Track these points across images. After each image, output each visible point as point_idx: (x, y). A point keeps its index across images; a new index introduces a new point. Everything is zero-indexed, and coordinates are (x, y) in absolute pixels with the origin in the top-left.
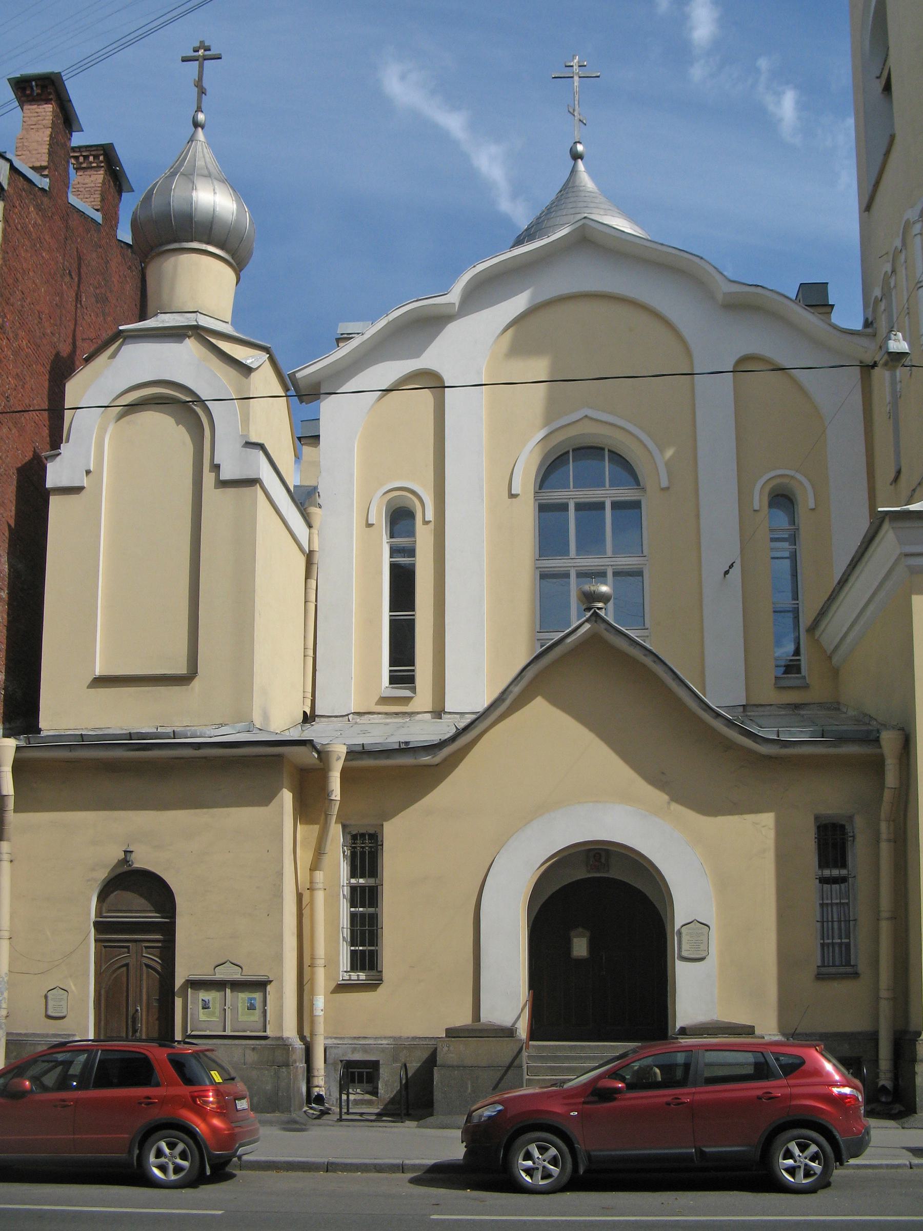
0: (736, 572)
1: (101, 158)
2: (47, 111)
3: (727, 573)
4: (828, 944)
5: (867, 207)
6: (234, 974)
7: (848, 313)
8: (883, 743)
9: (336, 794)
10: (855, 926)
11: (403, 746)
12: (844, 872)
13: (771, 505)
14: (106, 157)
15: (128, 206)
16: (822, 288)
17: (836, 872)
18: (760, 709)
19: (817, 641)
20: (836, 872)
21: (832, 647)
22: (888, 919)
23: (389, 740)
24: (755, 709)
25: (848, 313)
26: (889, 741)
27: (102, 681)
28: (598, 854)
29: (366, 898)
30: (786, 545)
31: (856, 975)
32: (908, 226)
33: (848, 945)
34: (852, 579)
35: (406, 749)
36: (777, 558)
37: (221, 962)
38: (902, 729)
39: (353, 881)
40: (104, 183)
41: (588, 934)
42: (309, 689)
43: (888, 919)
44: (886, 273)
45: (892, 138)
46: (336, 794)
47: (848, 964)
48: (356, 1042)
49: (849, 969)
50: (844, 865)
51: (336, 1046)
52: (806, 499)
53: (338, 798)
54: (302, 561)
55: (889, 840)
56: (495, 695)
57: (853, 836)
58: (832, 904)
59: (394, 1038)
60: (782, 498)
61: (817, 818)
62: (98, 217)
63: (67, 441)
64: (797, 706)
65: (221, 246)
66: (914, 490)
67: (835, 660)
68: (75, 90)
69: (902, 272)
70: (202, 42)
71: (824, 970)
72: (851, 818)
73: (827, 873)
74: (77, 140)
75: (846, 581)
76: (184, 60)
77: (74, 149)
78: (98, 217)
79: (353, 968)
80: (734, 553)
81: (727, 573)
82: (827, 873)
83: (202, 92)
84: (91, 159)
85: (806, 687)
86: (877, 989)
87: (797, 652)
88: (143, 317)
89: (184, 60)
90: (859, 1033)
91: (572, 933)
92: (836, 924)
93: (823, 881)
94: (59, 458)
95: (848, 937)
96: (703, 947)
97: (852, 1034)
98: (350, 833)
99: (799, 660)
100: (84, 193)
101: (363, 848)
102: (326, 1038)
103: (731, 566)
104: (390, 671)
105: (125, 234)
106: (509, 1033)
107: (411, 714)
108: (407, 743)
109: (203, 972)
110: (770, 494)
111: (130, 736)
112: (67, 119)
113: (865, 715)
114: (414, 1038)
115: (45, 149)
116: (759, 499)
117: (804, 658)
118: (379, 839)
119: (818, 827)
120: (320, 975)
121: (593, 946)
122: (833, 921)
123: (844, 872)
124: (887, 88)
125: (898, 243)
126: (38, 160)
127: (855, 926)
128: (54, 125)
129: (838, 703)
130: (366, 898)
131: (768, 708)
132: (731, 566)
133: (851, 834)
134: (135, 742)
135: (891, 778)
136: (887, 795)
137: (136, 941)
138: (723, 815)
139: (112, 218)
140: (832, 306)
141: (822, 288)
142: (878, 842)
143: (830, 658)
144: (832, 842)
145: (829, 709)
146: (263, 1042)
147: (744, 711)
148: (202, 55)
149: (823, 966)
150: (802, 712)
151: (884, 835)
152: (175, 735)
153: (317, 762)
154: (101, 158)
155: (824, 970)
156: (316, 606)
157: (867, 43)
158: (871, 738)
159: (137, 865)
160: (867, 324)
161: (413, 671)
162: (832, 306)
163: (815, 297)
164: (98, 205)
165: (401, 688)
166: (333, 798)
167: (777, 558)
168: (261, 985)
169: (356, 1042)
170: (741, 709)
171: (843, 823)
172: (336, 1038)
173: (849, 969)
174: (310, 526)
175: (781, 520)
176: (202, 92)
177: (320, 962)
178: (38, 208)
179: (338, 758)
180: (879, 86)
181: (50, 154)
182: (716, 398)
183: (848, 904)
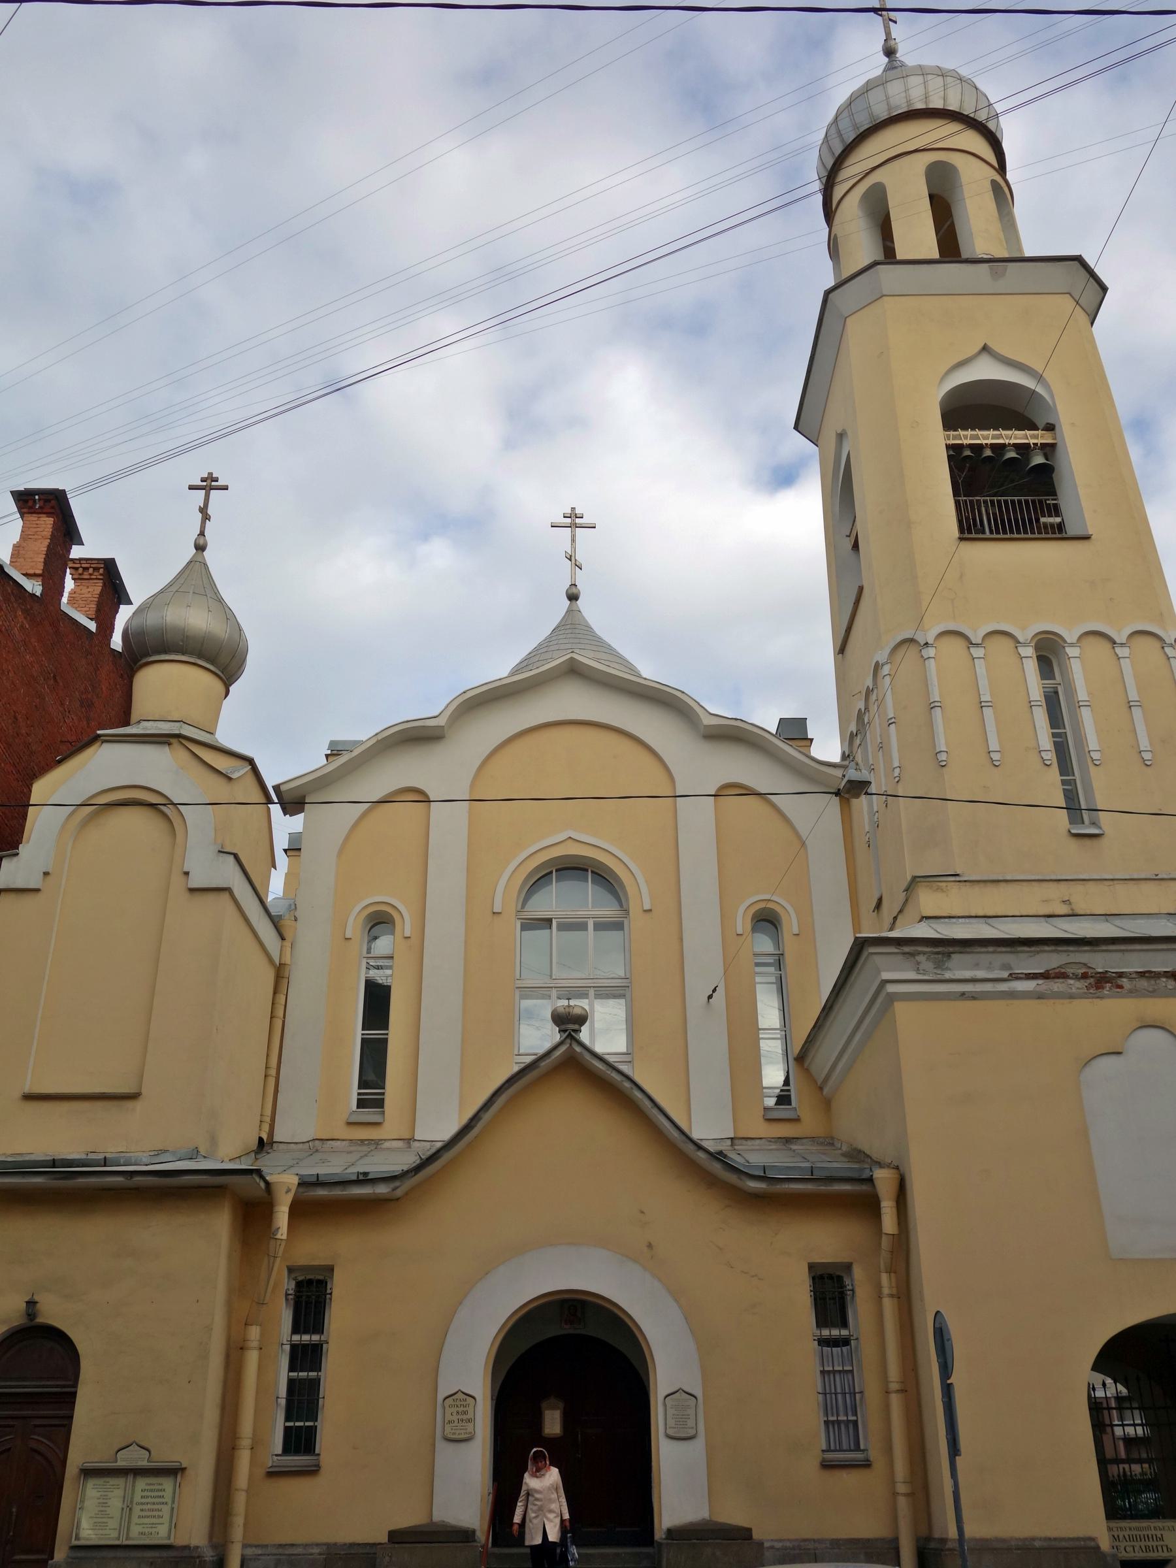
0: (720, 996)
1: (101, 571)
2: (47, 523)
3: (710, 997)
4: (833, 1422)
5: (842, 649)
6: (136, 1458)
7: (827, 747)
8: (878, 1184)
9: (283, 1232)
10: (862, 1399)
11: (361, 1177)
12: (844, 1332)
13: (754, 929)
14: (108, 572)
15: (124, 615)
16: (802, 722)
17: (835, 1332)
18: (749, 1142)
19: (807, 1070)
20: (835, 1332)
21: (823, 1076)
22: (898, 1391)
23: (350, 1170)
24: (744, 1142)
25: (827, 747)
26: (884, 1179)
27: (29, 1097)
28: (573, 1307)
29: (306, 1357)
30: (772, 969)
31: (866, 1465)
32: (877, 667)
33: (855, 1423)
34: (836, 1008)
35: (364, 1179)
36: (303, 1400)
37: (123, 1445)
38: (897, 1168)
39: (296, 1338)
40: (101, 595)
41: (561, 1405)
42: (268, 1112)
43: (898, 1391)
44: (860, 710)
45: (861, 589)
46: (283, 1232)
47: (857, 1448)
48: (280, 1551)
49: (859, 1456)
50: (844, 1324)
51: (256, 1558)
52: (791, 924)
53: (284, 1237)
54: (270, 975)
55: (891, 1296)
56: (465, 1121)
57: (853, 1290)
58: (834, 1372)
59: (328, 1545)
60: (767, 920)
61: (812, 1267)
62: (92, 626)
63: (28, 842)
64: (788, 1140)
65: (212, 662)
66: (895, 918)
67: (826, 1091)
68: (77, 506)
69: (873, 708)
70: (210, 474)
71: (576, 1027)
72: (848, 1267)
73: (825, 1332)
74: (76, 552)
75: (831, 1008)
76: (191, 488)
77: (73, 560)
78: (92, 626)
79: (287, 1450)
80: (716, 976)
81: (710, 997)
82: (825, 1332)
83: (206, 517)
84: (91, 570)
85: (797, 1120)
86: (893, 1482)
87: (787, 1082)
88: (127, 723)
89: (191, 488)
90: (877, 1540)
91: (544, 1405)
92: (840, 1396)
93: (823, 1342)
94: (15, 859)
95: (856, 1415)
96: (691, 1423)
97: (868, 1540)
98: (295, 1279)
99: (789, 1091)
100: (74, 599)
101: (308, 1297)
102: (245, 1546)
103: (714, 990)
104: (359, 1094)
105: (117, 642)
106: (465, 1536)
107: (377, 1143)
108: (366, 1174)
109: (96, 1460)
110: (752, 919)
111: (54, 1163)
112: (67, 532)
113: (860, 1151)
114: (352, 1545)
115: (41, 558)
116: (742, 923)
117: (792, 1087)
118: (329, 1287)
119: (813, 1278)
120: (244, 1460)
121: (568, 1420)
122: (836, 1394)
123: (844, 1332)
124: (856, 546)
125: (869, 682)
126: (32, 567)
127: (862, 1399)
128: (53, 537)
129: (832, 1138)
130: (306, 1357)
131: (758, 1142)
132: (714, 990)
133: (850, 1287)
134: (56, 1167)
135: (889, 1222)
136: (885, 1243)
137: (24, 1418)
138: (883, 1563)
139: (106, 627)
140: (812, 740)
141: (802, 722)
142: (880, 1298)
143: (821, 1089)
144: (830, 1292)
145: (822, 1144)
146: (165, 1554)
147: (732, 1145)
148: (209, 484)
149: (829, 1450)
150: (794, 1147)
151: (886, 1291)
152: (105, 1162)
153: (265, 1195)
154: (101, 571)
155: (576, 1027)
156: (284, 1022)
157: (837, 509)
158: (864, 1176)
159: (40, 1320)
160: (844, 757)
161: (383, 1094)
162: (812, 740)
163: (795, 731)
164: (92, 613)
165: (374, 1113)
166: (279, 1236)
167: (303, 1400)
168: (174, 1472)
169: (280, 1551)
170: (729, 1142)
171: (838, 1273)
172: (257, 1546)
173: (859, 1456)
174: (283, 939)
175: (764, 944)
176: (206, 517)
177: (246, 1442)
178: (26, 612)
179: (288, 1191)
180: (848, 544)
181: (45, 563)
182: (697, 819)
183: (852, 1372)
